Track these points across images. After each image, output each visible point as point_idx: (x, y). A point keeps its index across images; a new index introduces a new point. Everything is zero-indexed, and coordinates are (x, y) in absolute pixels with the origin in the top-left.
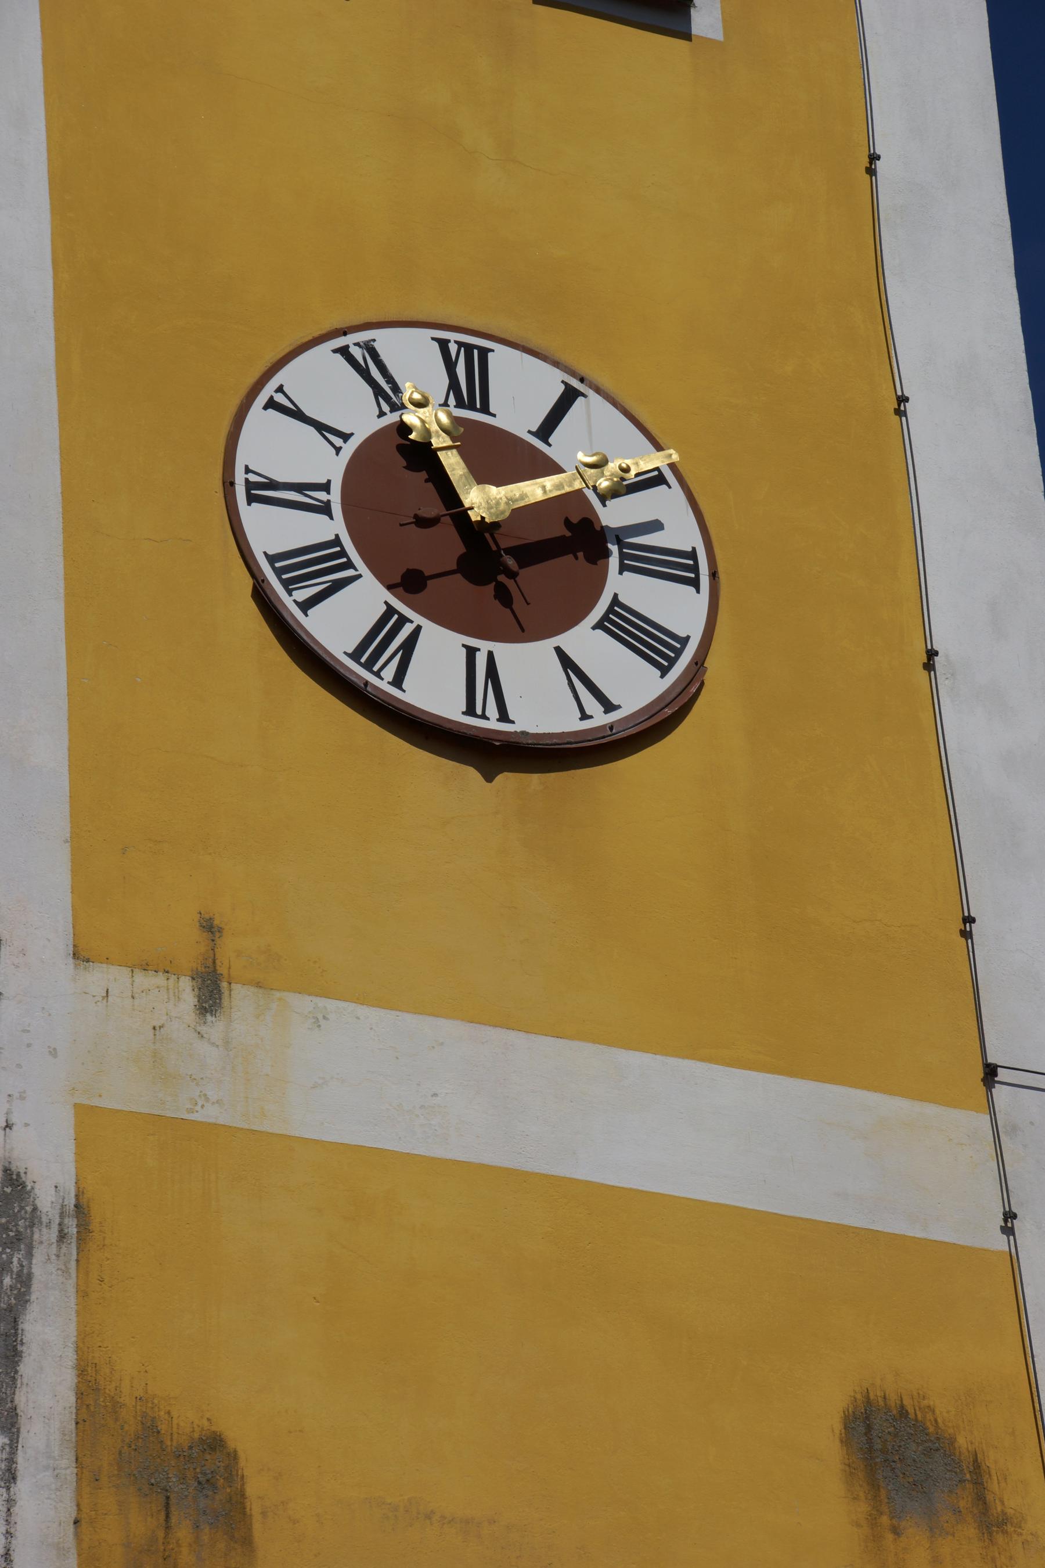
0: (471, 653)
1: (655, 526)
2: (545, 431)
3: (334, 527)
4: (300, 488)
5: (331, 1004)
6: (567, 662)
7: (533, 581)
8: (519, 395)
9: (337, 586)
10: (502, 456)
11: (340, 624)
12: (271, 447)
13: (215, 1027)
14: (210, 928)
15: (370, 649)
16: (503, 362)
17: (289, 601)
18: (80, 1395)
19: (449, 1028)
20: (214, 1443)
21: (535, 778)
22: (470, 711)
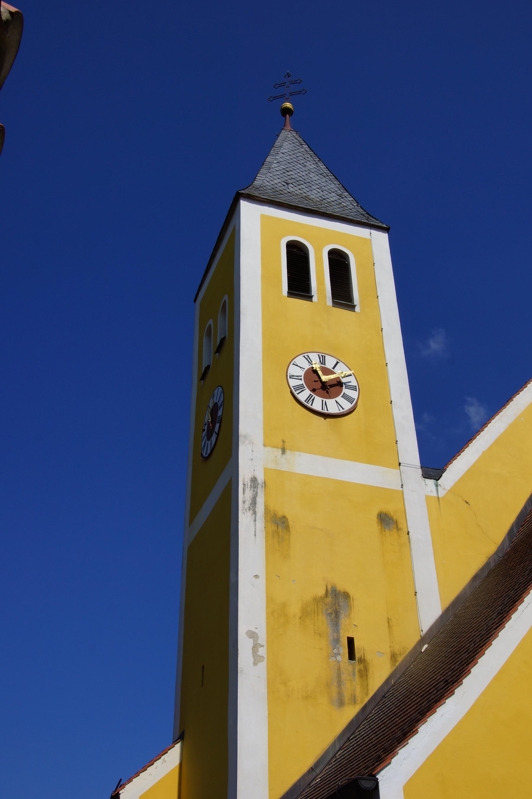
0: (323, 401)
1: (350, 382)
2: (334, 368)
3: (303, 382)
4: (297, 376)
5: (302, 453)
6: (337, 402)
7: (332, 390)
8: (330, 363)
9: (313, 400)
10: (327, 371)
11: (303, 396)
12: (293, 370)
13: (284, 456)
14: (283, 441)
15: (307, 400)
16: (327, 357)
17: (295, 393)
18: (265, 509)
19: (319, 457)
20: (284, 517)
21: (332, 419)
22: (322, 409)
